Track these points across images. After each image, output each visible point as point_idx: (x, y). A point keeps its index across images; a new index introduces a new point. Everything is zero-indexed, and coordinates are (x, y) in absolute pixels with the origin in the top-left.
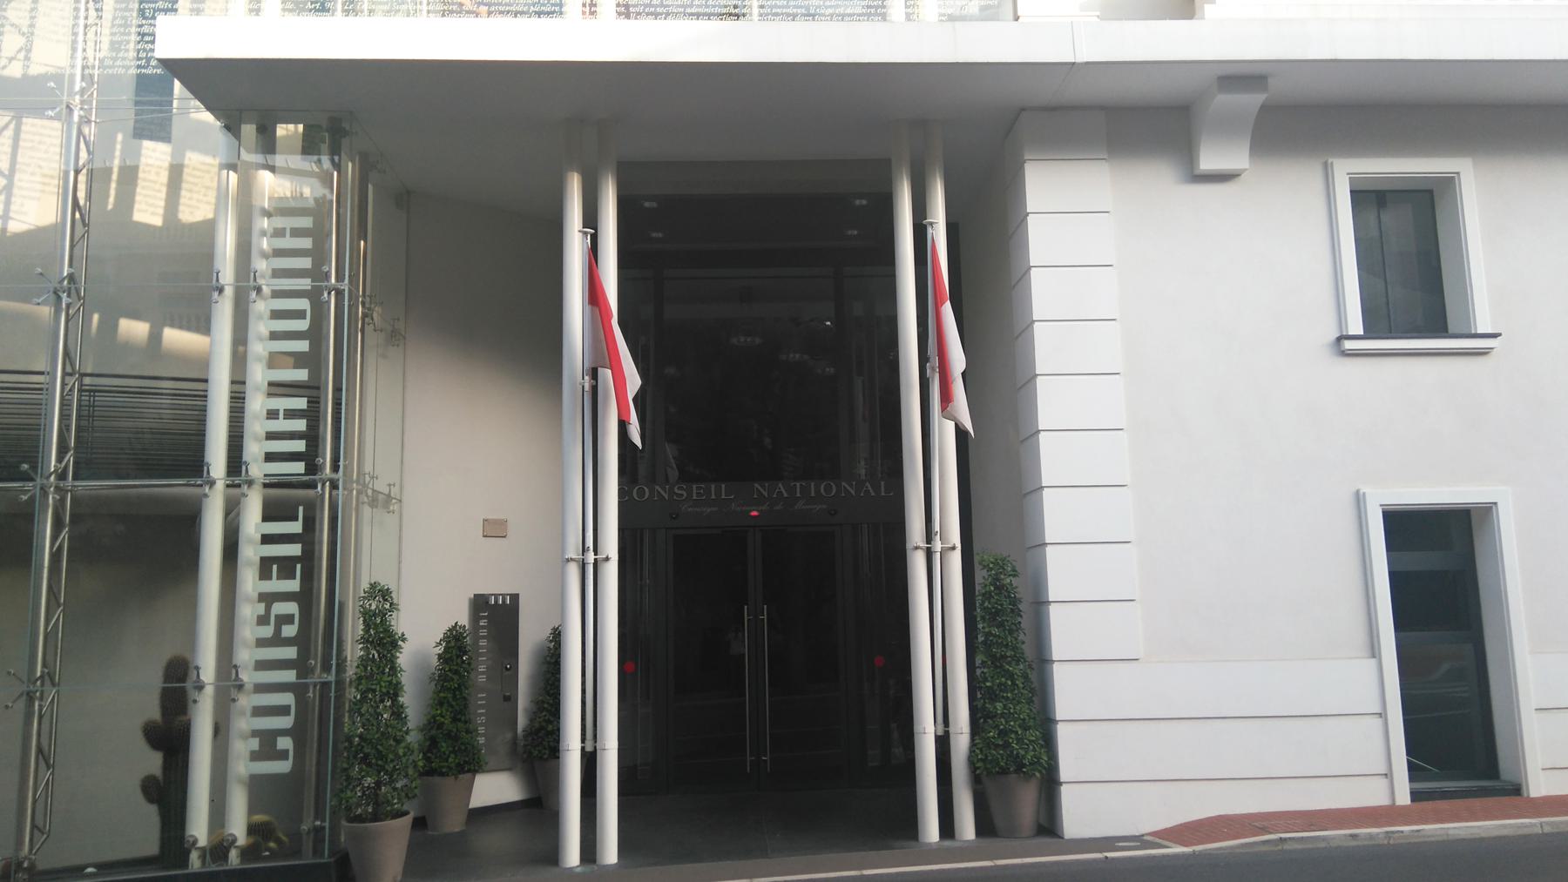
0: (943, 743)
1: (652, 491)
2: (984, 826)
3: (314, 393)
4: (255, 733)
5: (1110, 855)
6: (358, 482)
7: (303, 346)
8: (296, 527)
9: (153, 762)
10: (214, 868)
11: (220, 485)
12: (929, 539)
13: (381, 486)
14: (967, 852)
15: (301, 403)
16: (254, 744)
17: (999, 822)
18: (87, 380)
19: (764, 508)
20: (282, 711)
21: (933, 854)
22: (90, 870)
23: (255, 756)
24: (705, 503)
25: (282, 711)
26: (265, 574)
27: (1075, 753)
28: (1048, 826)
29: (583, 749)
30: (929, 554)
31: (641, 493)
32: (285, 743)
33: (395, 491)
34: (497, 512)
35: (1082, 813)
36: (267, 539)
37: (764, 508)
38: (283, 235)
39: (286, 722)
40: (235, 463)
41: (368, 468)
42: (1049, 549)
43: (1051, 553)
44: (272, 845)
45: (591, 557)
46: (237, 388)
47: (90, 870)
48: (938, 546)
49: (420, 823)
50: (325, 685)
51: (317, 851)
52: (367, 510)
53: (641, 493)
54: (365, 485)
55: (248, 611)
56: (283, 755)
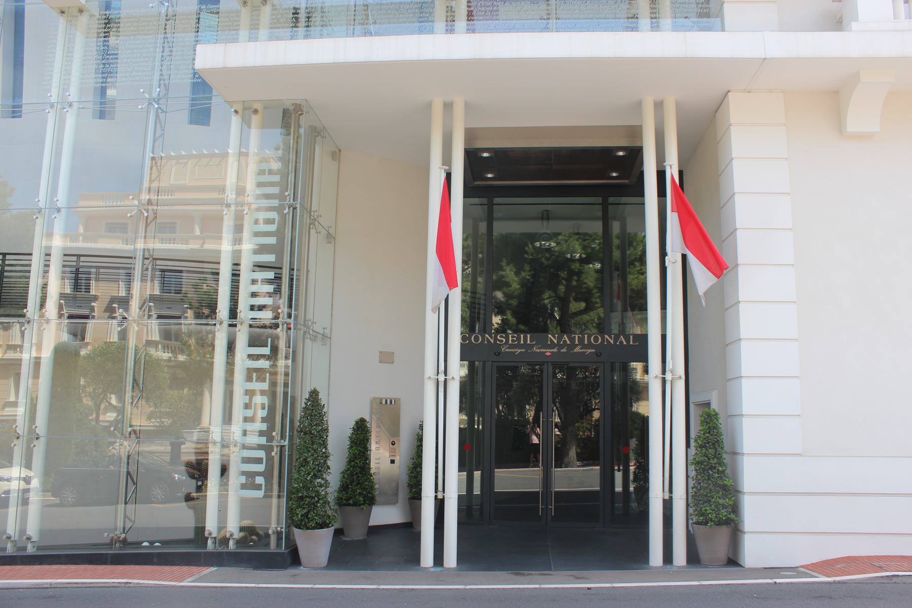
0: (668, 506)
1: (483, 338)
2: (693, 558)
3: (278, 271)
4: (244, 473)
5: (778, 581)
6: (305, 325)
7: (272, 240)
8: (266, 351)
9: (191, 485)
10: (220, 550)
11: (225, 324)
12: (664, 371)
13: (317, 328)
14: (679, 574)
15: (271, 275)
16: (243, 479)
17: (704, 555)
18: (158, 262)
19: (555, 350)
20: (258, 461)
21: (657, 574)
22: (157, 544)
23: (244, 487)
24: (516, 344)
25: (258, 461)
26: (249, 379)
27: (754, 514)
28: (733, 561)
29: (436, 496)
30: (664, 381)
31: (476, 339)
32: (260, 480)
33: (327, 331)
34: (405, 359)
35: (755, 551)
36: (251, 357)
37: (555, 350)
38: (264, 174)
39: (261, 468)
40: (233, 313)
41: (310, 316)
42: (744, 381)
43: (745, 384)
44: (254, 537)
45: (442, 378)
46: (236, 267)
47: (157, 544)
48: (669, 376)
49: (338, 533)
50: (282, 447)
51: (279, 544)
52: (308, 342)
53: (476, 339)
54: (308, 328)
55: (239, 400)
56: (258, 487)
